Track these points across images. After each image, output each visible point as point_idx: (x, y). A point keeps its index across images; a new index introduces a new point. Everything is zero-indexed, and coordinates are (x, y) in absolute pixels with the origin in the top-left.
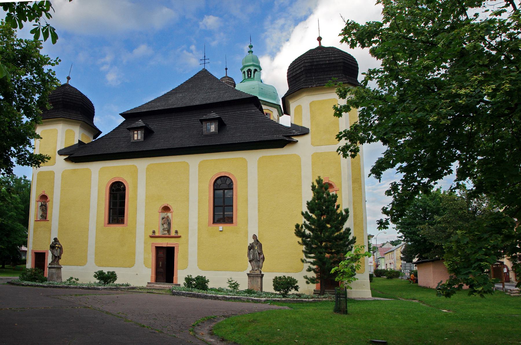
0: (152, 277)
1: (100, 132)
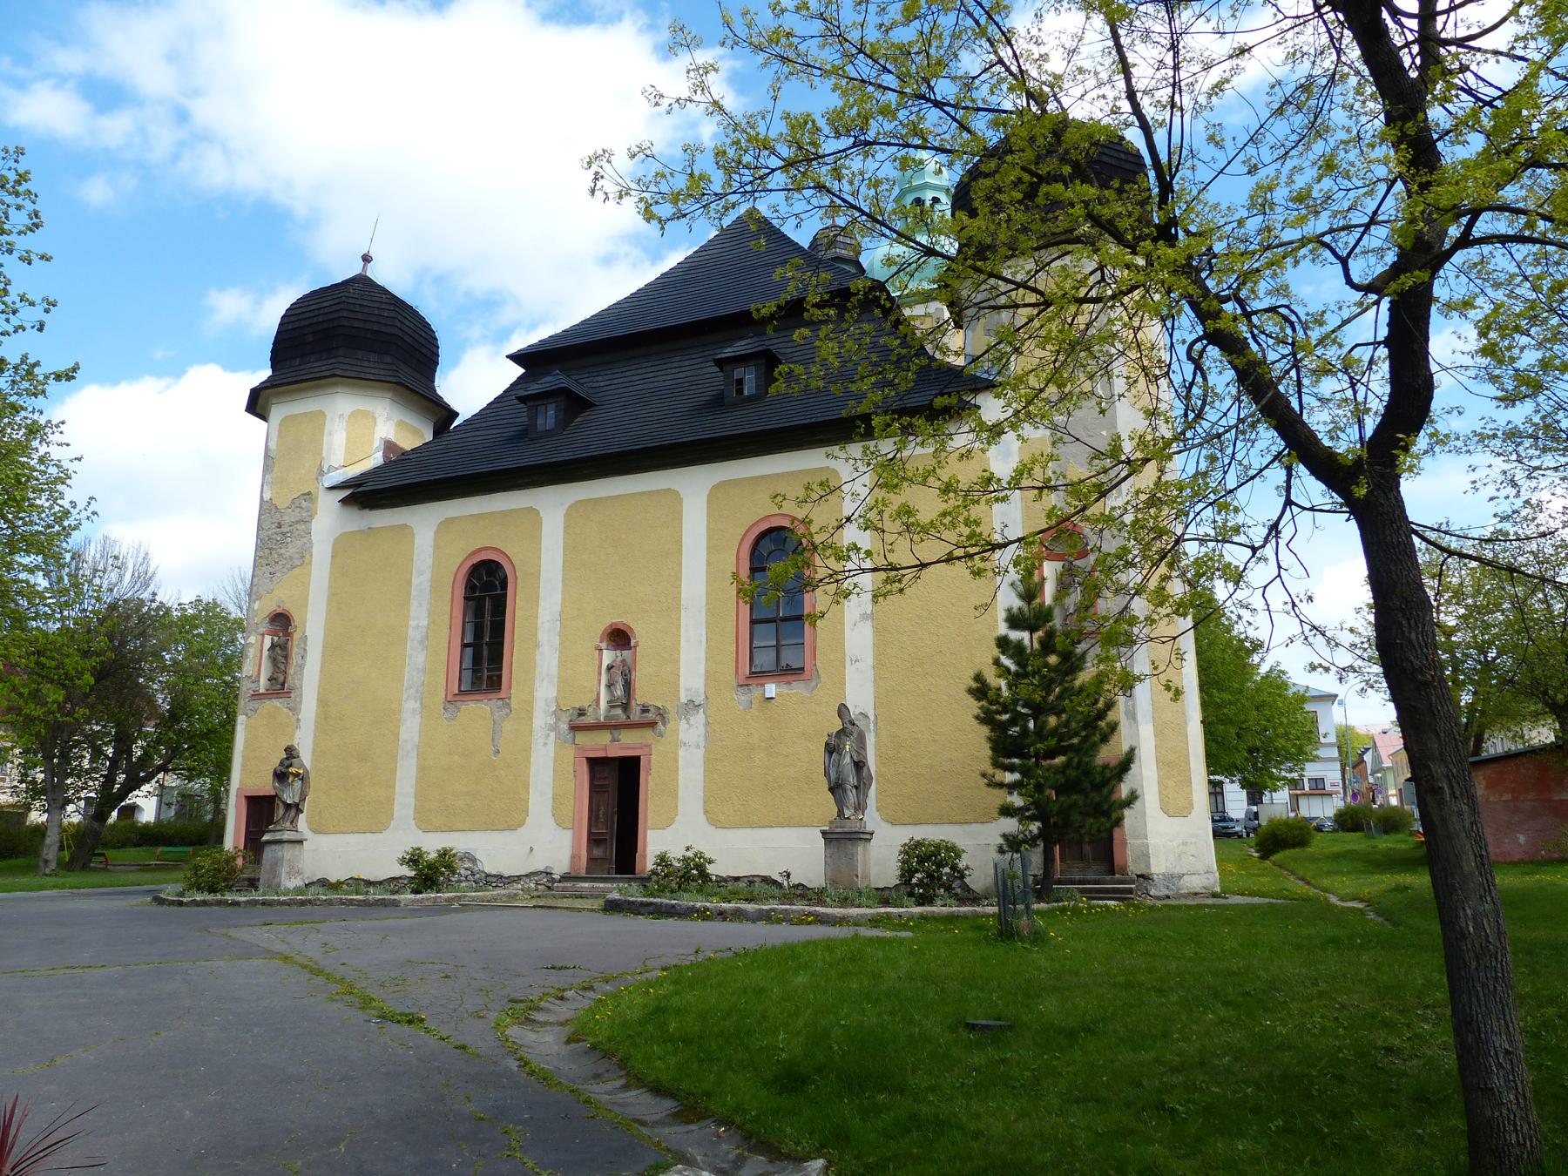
1: (456, 415)
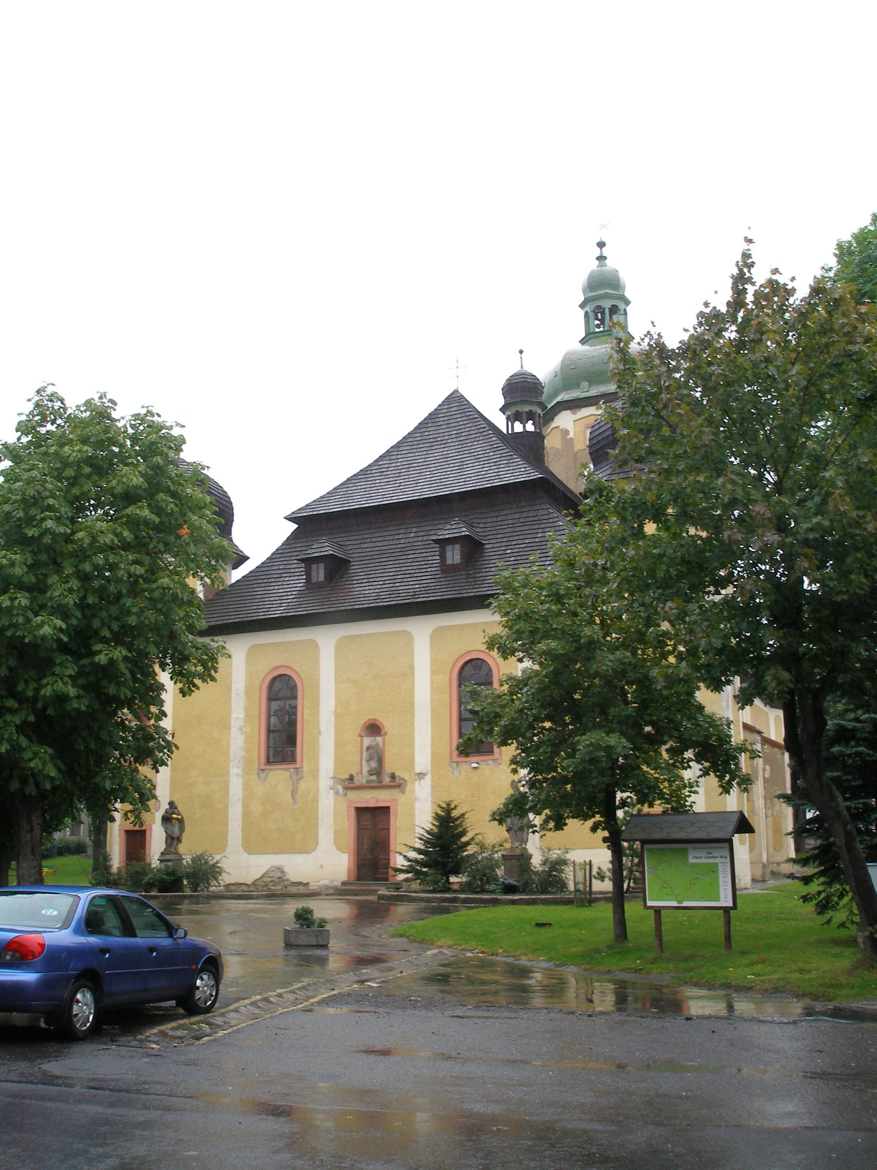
0: (349, 870)
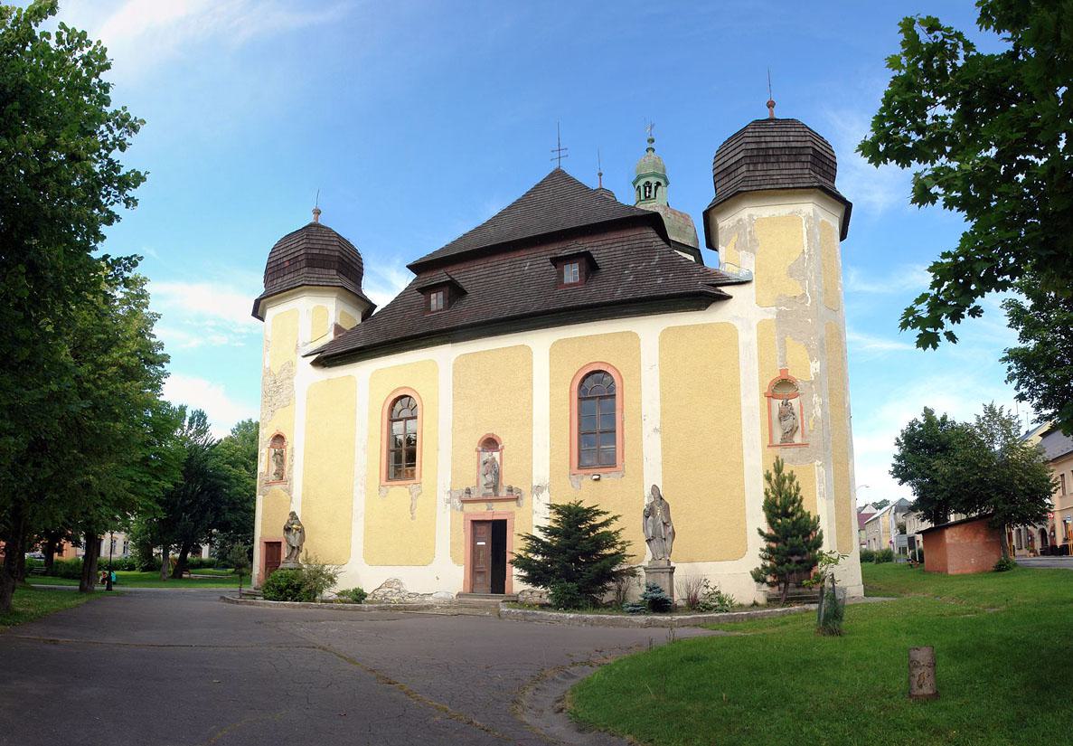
1: (376, 306)
